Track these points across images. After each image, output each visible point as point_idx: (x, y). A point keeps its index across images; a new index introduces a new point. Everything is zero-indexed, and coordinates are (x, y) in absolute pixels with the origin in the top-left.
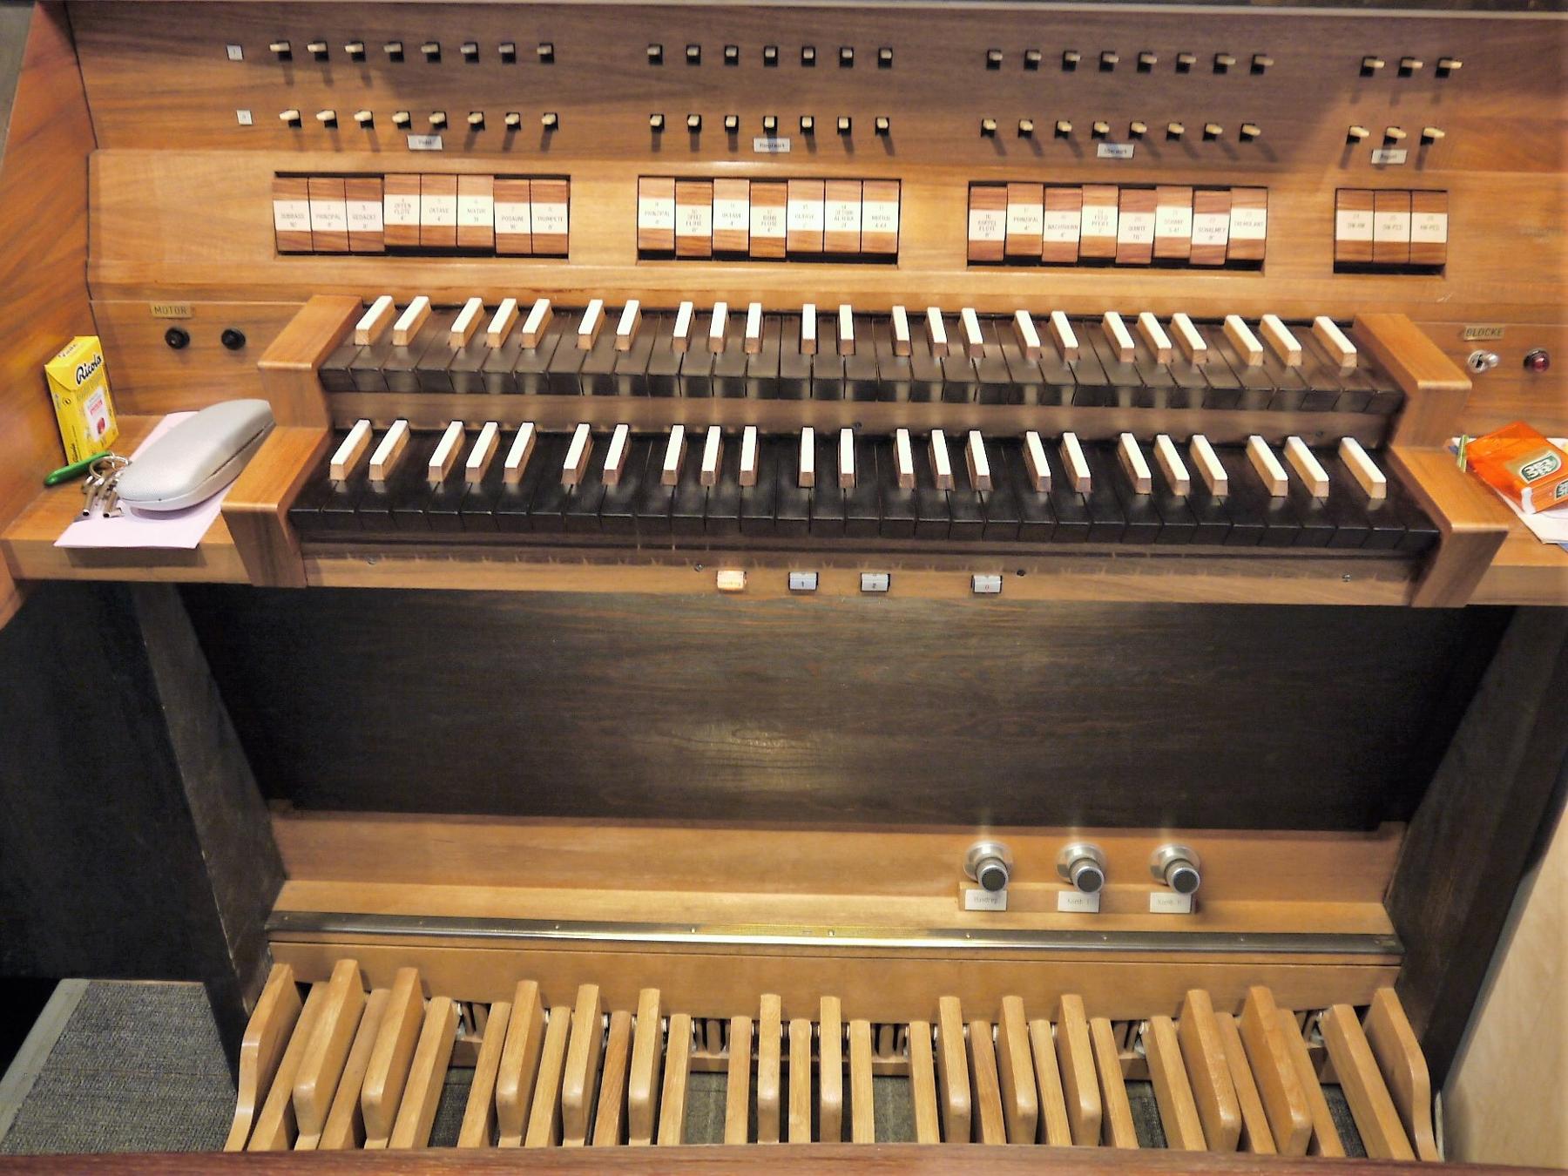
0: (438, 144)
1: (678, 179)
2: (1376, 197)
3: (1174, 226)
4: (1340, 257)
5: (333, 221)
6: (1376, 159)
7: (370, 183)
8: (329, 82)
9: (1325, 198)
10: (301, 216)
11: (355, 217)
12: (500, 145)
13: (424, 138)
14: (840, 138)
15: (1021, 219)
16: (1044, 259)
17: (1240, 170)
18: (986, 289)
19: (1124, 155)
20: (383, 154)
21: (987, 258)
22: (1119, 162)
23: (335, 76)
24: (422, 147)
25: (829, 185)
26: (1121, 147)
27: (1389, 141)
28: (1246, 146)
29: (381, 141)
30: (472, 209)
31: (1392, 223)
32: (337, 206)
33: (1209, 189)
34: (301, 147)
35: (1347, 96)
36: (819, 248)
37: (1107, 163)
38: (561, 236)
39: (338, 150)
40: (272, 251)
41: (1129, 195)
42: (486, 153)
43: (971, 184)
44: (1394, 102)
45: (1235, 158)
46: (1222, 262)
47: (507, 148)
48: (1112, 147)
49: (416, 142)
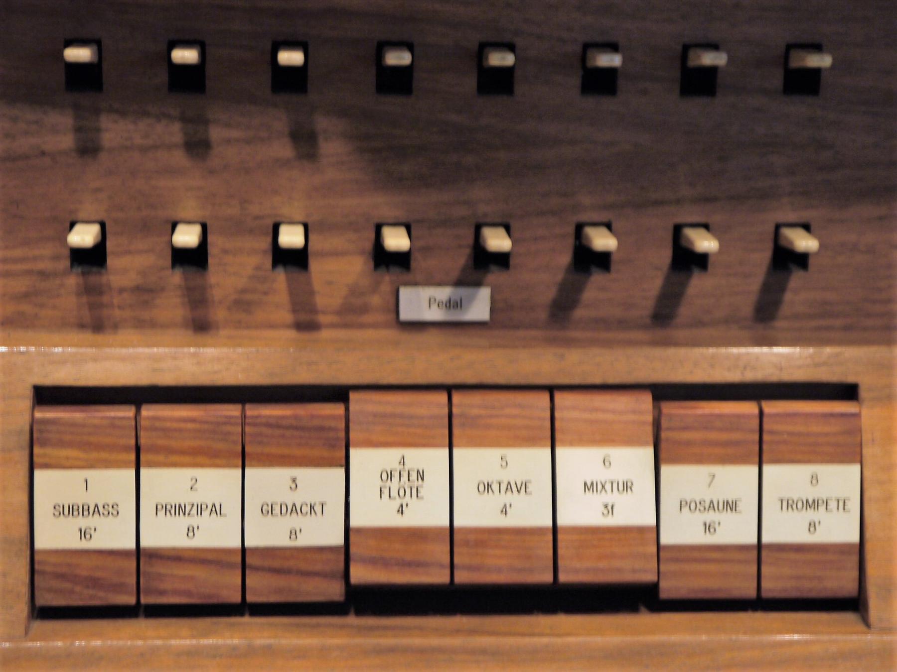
0: (479, 306)
5: (206, 520)
7: (305, 417)
8: (197, 147)
10: (112, 510)
11: (268, 510)
12: (746, 305)
13: (444, 293)
16: (664, 595)
20: (325, 334)
23: (216, 133)
24: (435, 314)
29: (320, 301)
30: (597, 486)
32: (217, 483)
34: (96, 323)
36: (440, 577)
38: (841, 549)
39: (201, 326)
40: (22, 608)
42: (612, 329)
47: (664, 316)
49: (420, 302)
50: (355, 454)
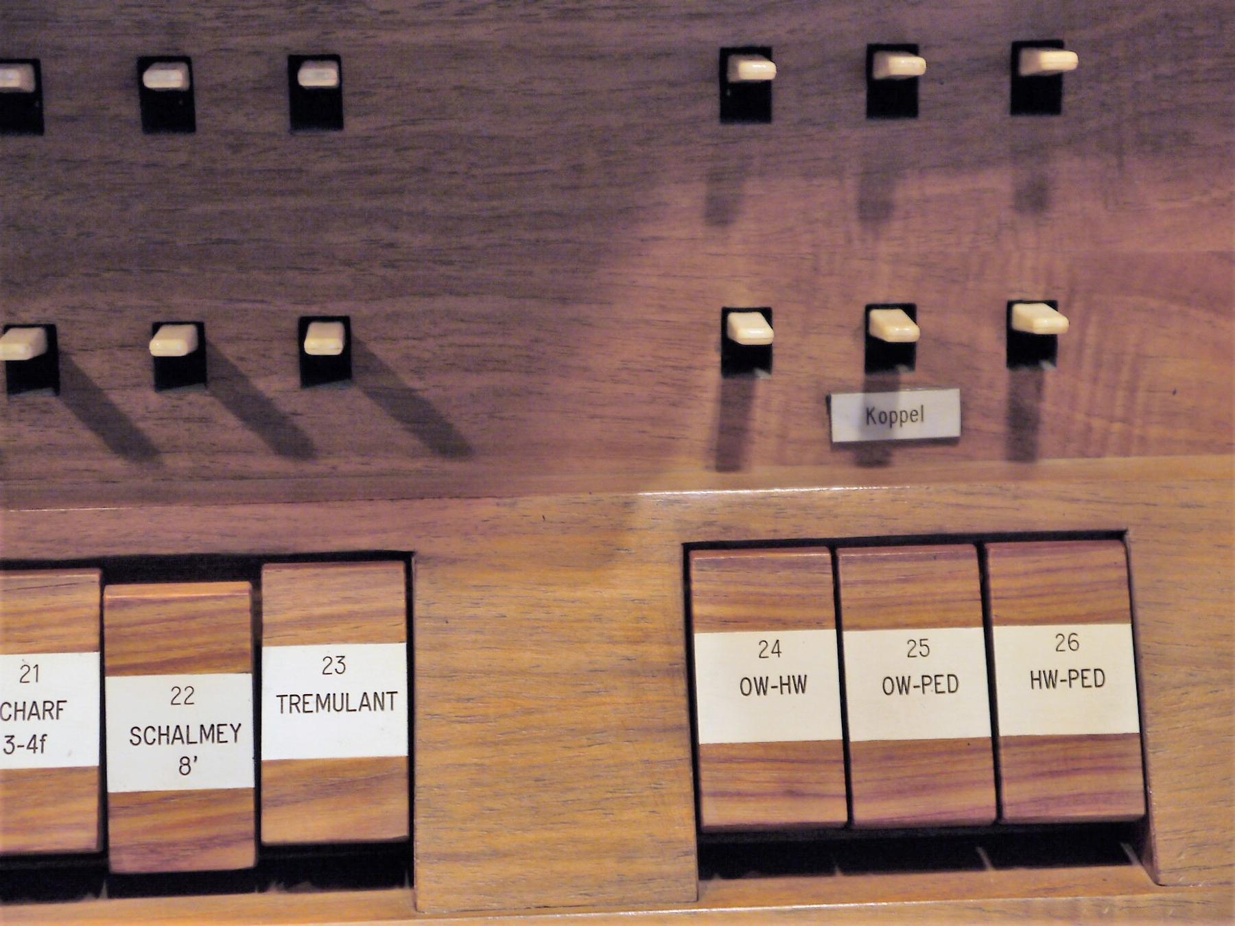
1: (117, 570)
2: (834, 575)
3: (23, 729)
4: (717, 814)
6: (847, 421)
9: (650, 584)
25: (854, 566)
27: (886, 360)
31: (915, 670)
35: (685, 198)
44: (874, 211)
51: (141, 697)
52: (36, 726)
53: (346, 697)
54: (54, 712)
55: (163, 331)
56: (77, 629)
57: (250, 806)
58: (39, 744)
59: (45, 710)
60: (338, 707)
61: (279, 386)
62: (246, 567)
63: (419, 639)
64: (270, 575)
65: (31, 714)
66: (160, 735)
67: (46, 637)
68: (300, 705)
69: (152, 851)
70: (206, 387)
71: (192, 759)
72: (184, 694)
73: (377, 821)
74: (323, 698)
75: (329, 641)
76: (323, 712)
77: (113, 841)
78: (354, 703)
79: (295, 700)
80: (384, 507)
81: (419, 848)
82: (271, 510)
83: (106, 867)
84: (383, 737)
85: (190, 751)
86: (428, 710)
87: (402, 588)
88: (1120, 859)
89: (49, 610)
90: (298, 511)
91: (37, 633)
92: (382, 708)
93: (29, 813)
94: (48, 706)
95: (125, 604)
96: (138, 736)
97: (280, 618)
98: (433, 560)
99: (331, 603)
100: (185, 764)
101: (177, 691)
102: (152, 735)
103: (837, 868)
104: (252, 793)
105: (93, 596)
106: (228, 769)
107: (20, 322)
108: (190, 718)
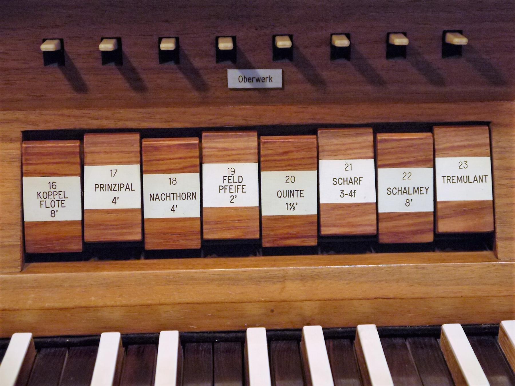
3: (347, 188)
14: (55, 72)
15: (111, 187)
17: (444, 99)
18: (53, 300)
19: (269, 85)
21: (57, 248)
22: (263, 95)
26: (263, 73)
28: (453, 62)
33: (401, 129)
37: (240, 96)
41: (277, 143)
43: (28, 136)
45: (440, 82)
46: (429, 238)
48: (249, 73)
50: (322, 163)
51: (390, 176)
52: (352, 187)
53: (468, 177)
54: (358, 182)
55: (104, 40)
56: (364, 150)
57: (432, 218)
58: (353, 194)
59: (355, 181)
60: (465, 181)
61: (434, 58)
62: (78, 135)
63: (494, 156)
64: (87, 138)
65: (126, 188)
66: (398, 191)
67: (354, 153)
68: (451, 180)
69: (395, 235)
70: (405, 58)
71: (56, 211)
72: (408, 176)
73: (480, 224)
74: (459, 178)
75: (461, 156)
76: (460, 183)
77: (380, 231)
78: (472, 179)
79: (449, 178)
80: (479, 104)
81: (498, 235)
82: (435, 105)
83: (143, 248)
84: (483, 192)
85: (409, 197)
86: (499, 183)
87: (488, 135)
88: (481, 248)
89: (354, 143)
90: (446, 106)
91: (351, 152)
92: (482, 182)
93: (351, 220)
94: (356, 179)
95: (386, 141)
96: (390, 192)
97: (441, 147)
98: (498, 125)
99: (461, 141)
100: (408, 202)
101: (405, 174)
102: (395, 191)
103: (142, 257)
104: (433, 213)
105: (371, 138)
106: (423, 204)
107: (336, 32)
108: (410, 184)
